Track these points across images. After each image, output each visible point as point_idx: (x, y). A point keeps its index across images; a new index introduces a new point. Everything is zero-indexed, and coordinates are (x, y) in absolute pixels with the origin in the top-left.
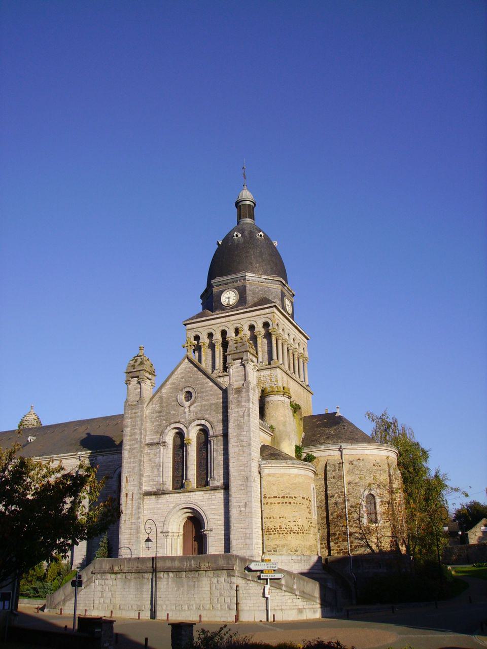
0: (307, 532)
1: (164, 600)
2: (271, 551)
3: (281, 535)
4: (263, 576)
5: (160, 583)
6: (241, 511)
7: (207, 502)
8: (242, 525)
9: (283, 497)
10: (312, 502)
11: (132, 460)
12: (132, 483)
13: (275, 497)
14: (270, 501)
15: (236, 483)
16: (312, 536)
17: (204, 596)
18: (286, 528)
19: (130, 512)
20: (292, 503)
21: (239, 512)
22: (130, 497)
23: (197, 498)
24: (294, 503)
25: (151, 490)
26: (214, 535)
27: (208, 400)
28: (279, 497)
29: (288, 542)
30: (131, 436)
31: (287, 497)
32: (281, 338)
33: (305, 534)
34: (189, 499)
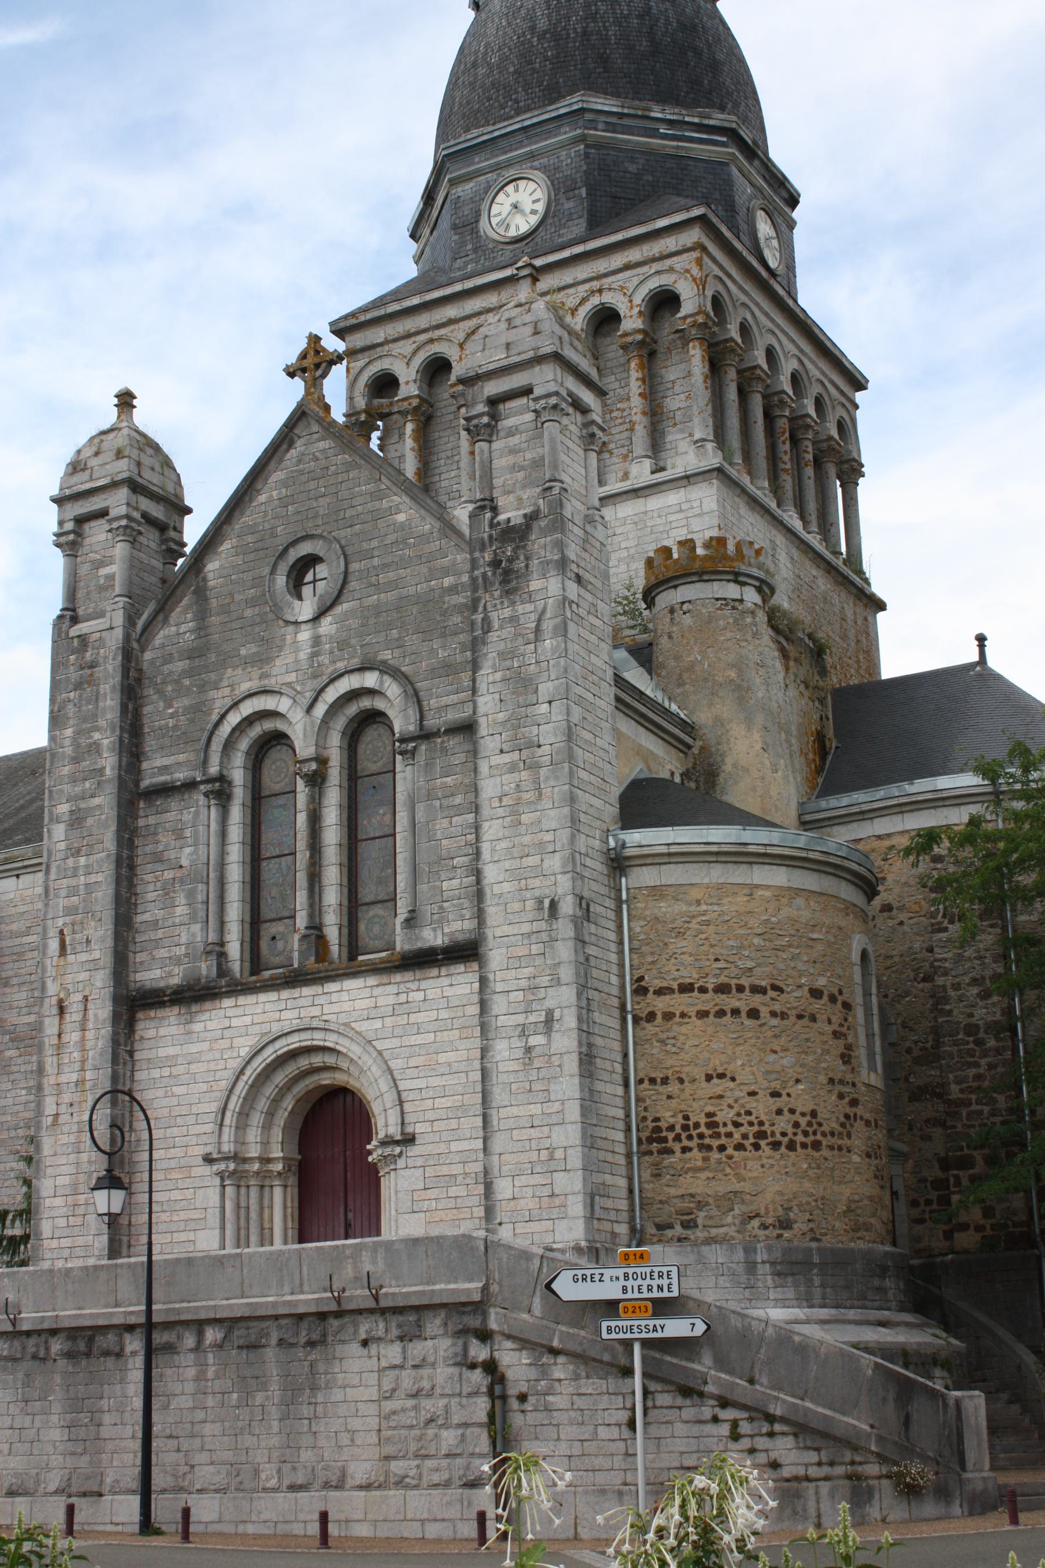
0: (836, 1141)
1: (185, 1447)
2: (671, 1226)
3: (715, 1155)
4: (609, 1330)
5: (169, 1372)
6: (529, 1050)
7: (389, 1021)
8: (536, 1109)
9: (722, 989)
10: (859, 1012)
11: (82, 860)
12: (84, 957)
13: (686, 988)
14: (661, 1004)
15: (507, 930)
16: (856, 1158)
17: (355, 1424)
18: (737, 1125)
19: (74, 1077)
20: (764, 1011)
21: (519, 1053)
22: (74, 1015)
23: (347, 1007)
24: (773, 1014)
25: (162, 984)
26: (420, 1162)
27: (394, 585)
28: (703, 990)
29: (746, 1186)
30: (76, 760)
31: (740, 989)
32: (732, 360)
33: (825, 1152)
34: (315, 1011)
